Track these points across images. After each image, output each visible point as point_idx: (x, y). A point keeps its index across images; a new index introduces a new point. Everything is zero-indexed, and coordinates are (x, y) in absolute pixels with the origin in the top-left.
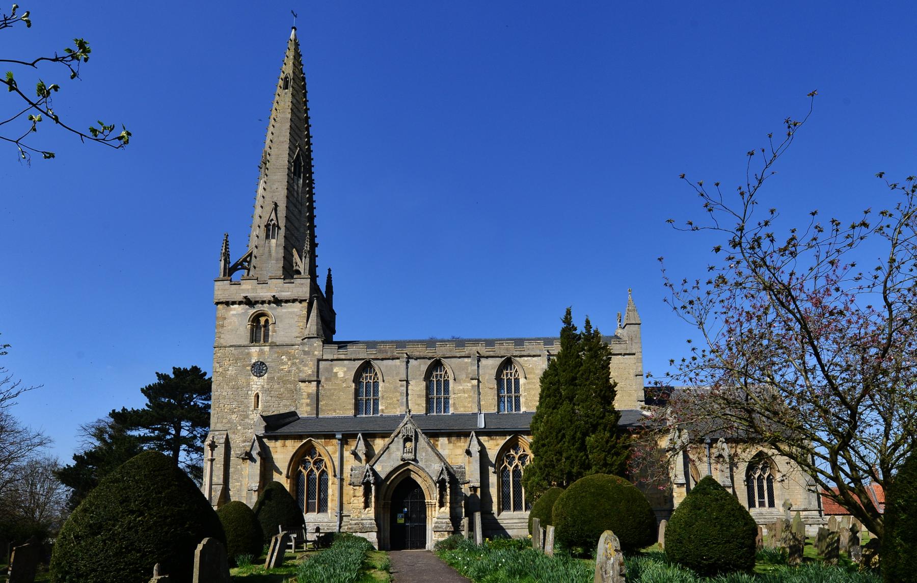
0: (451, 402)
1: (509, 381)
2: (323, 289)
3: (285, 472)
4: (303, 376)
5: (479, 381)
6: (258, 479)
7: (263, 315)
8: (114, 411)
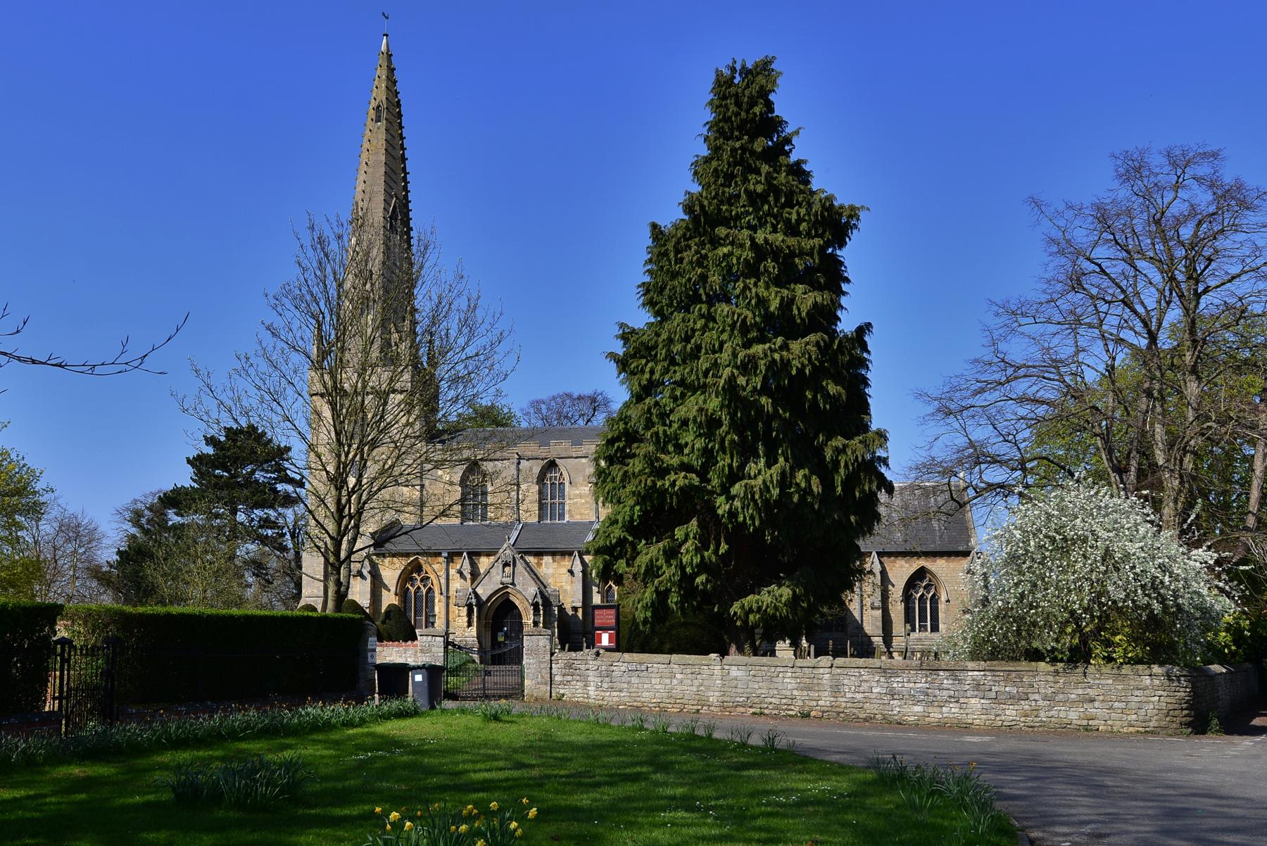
3: (393, 589)
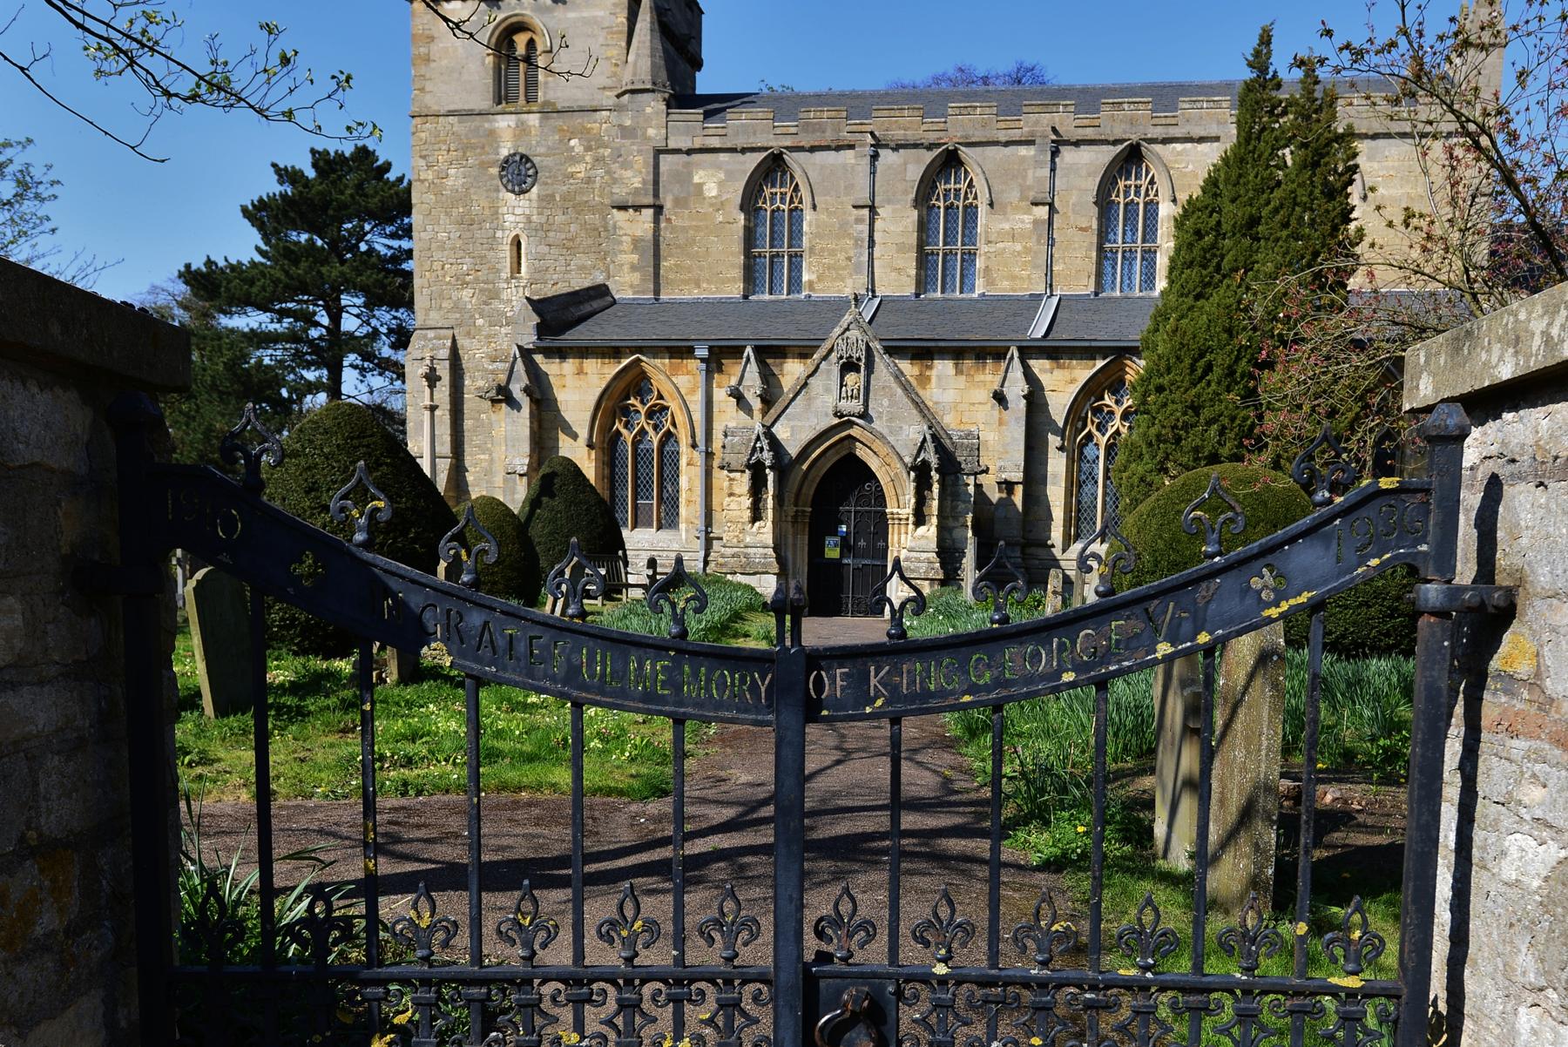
0: (980, 263)
3: (583, 434)
4: (621, 193)
5: (1052, 209)
8: (188, 266)
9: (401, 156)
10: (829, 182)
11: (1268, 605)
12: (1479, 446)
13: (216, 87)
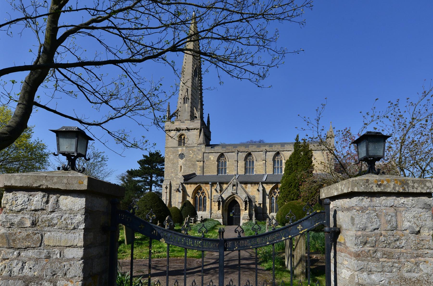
1: (278, 161)
2: (206, 123)
3: (191, 196)
4: (198, 159)
6: (181, 199)
7: (183, 135)
9: (163, 154)
10: (231, 158)
11: (300, 231)
12: (332, 205)
13: (135, 146)
